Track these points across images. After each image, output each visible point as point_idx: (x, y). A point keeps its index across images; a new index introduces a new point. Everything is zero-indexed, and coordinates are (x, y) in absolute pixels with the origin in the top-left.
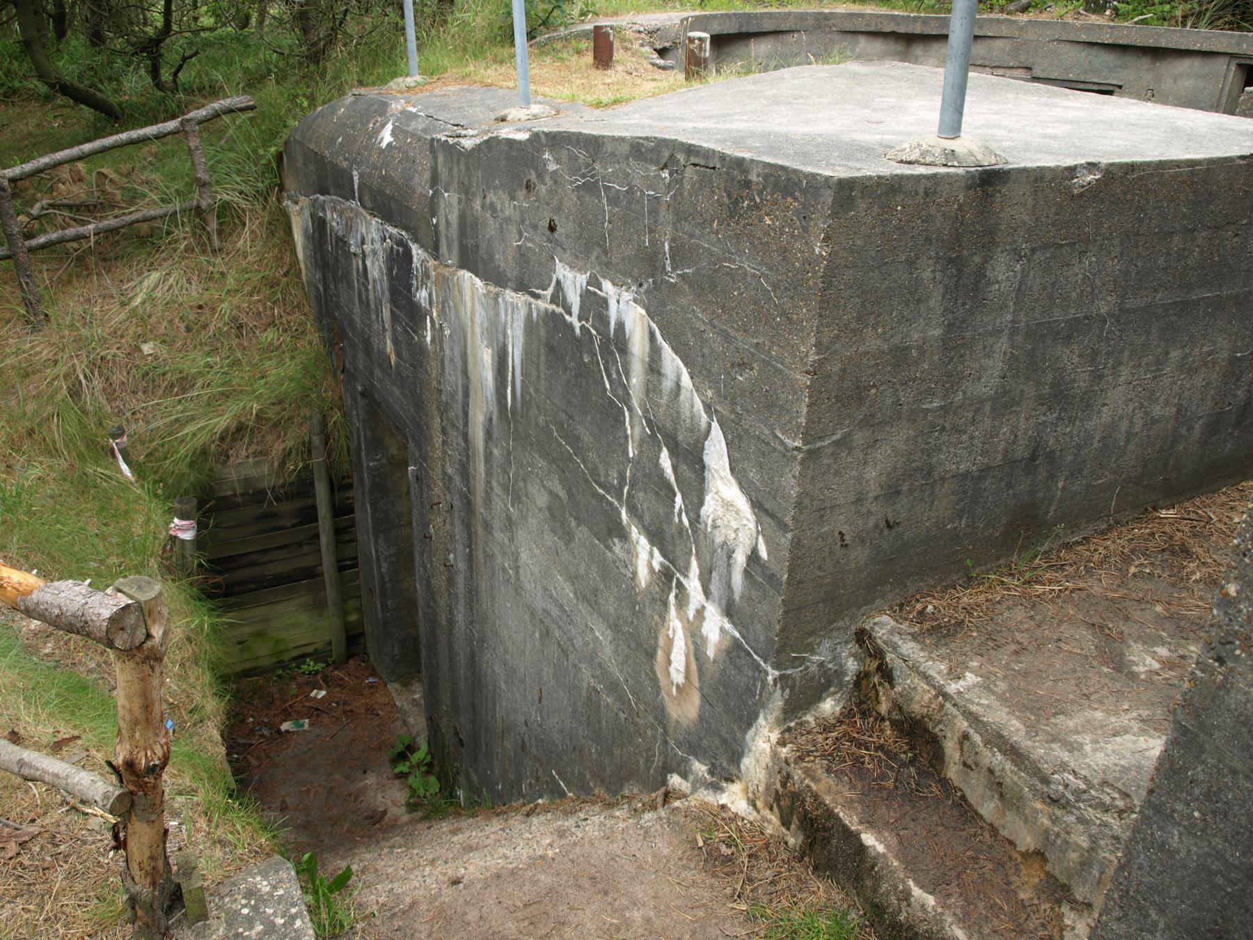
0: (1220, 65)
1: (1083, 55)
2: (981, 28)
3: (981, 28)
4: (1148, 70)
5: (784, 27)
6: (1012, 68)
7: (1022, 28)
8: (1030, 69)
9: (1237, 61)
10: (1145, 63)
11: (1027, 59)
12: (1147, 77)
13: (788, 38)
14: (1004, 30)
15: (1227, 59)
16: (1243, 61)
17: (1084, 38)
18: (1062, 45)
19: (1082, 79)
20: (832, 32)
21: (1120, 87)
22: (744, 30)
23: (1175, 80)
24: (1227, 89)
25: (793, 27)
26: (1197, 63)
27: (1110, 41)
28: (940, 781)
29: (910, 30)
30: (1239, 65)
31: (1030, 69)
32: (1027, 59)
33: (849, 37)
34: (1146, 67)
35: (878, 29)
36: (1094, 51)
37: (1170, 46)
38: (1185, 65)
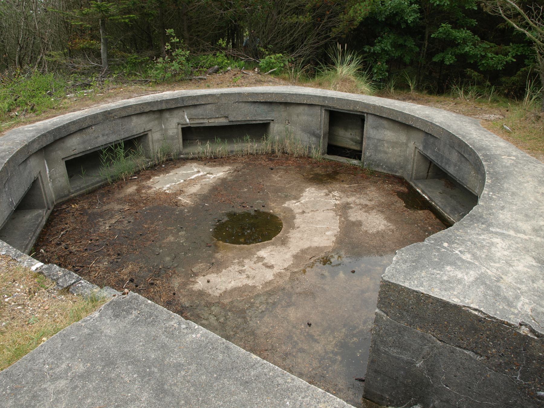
0: (317, 110)
1: (252, 108)
2: (197, 100)
3: (197, 100)
4: (284, 111)
5: (84, 126)
6: (218, 118)
7: (218, 98)
8: (227, 117)
9: (324, 108)
10: (282, 108)
11: (225, 113)
12: (284, 114)
13: (90, 130)
14: (210, 100)
15: (320, 107)
16: (327, 109)
17: (250, 100)
18: (240, 104)
19: (254, 119)
20: (115, 120)
21: (273, 120)
22: (58, 138)
23: (298, 116)
24: (323, 121)
25: (90, 124)
26: (306, 108)
27: (264, 101)
28: (229, 157)
29: (160, 108)
30: (325, 110)
31: (227, 117)
32: (225, 113)
33: (126, 119)
34: (283, 110)
35: (142, 110)
36: (257, 105)
37: (292, 102)
38: (301, 109)
